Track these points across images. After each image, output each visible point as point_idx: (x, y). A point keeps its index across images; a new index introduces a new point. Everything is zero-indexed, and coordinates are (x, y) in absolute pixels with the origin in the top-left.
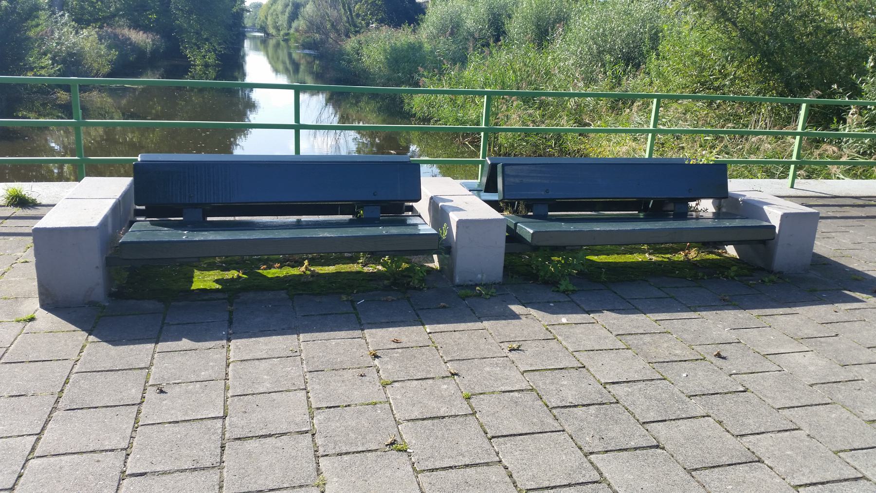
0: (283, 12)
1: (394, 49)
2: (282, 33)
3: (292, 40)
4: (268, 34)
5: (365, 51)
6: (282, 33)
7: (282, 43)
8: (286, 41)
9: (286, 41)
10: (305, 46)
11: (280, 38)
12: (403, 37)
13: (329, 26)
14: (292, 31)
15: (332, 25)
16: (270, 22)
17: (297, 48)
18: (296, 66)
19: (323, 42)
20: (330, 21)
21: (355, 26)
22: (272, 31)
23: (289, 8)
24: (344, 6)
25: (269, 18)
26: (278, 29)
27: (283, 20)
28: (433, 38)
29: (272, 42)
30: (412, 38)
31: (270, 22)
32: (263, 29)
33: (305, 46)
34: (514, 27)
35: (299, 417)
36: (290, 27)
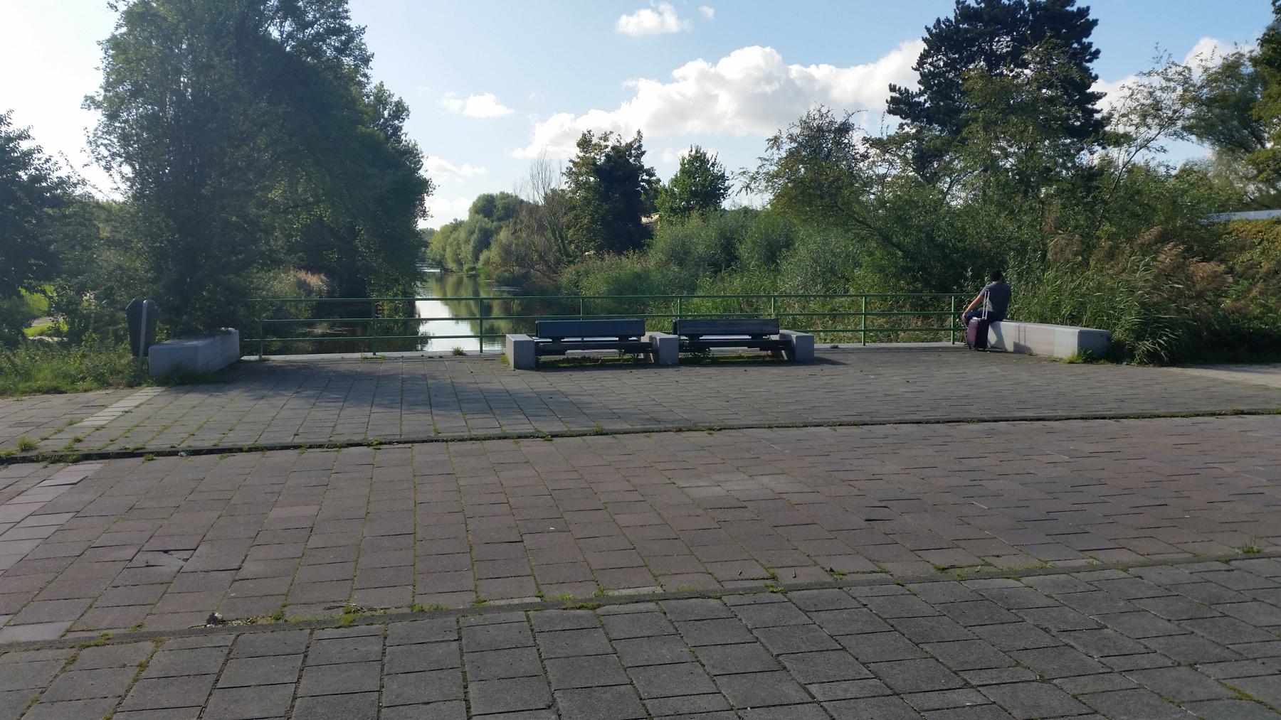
0: (467, 241)
1: (617, 280)
2: (466, 267)
3: (482, 276)
4: (446, 271)
5: (584, 283)
6: (466, 267)
7: (465, 279)
8: (474, 278)
9: (474, 278)
10: (502, 282)
11: (464, 274)
12: (630, 264)
13: (535, 257)
14: (479, 265)
15: (540, 256)
16: (448, 254)
17: (489, 285)
18: (486, 310)
19: (526, 276)
20: (537, 251)
21: (568, 255)
22: (451, 265)
23: (475, 236)
24: (554, 235)
25: (448, 250)
26: (459, 263)
27: (467, 251)
28: (662, 265)
29: (452, 280)
30: (638, 268)
31: (448, 254)
32: (440, 264)
33: (502, 282)
34: (743, 250)
35: (393, 686)
36: (477, 259)
